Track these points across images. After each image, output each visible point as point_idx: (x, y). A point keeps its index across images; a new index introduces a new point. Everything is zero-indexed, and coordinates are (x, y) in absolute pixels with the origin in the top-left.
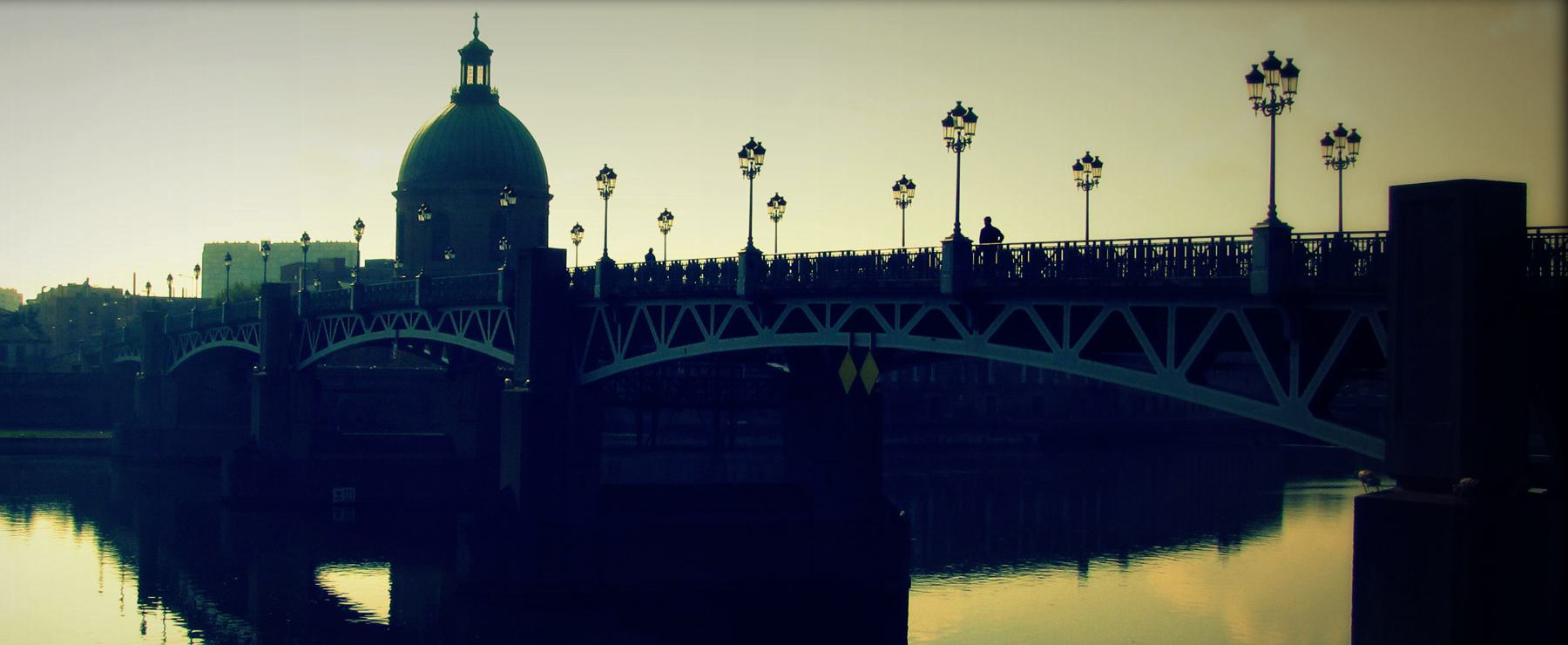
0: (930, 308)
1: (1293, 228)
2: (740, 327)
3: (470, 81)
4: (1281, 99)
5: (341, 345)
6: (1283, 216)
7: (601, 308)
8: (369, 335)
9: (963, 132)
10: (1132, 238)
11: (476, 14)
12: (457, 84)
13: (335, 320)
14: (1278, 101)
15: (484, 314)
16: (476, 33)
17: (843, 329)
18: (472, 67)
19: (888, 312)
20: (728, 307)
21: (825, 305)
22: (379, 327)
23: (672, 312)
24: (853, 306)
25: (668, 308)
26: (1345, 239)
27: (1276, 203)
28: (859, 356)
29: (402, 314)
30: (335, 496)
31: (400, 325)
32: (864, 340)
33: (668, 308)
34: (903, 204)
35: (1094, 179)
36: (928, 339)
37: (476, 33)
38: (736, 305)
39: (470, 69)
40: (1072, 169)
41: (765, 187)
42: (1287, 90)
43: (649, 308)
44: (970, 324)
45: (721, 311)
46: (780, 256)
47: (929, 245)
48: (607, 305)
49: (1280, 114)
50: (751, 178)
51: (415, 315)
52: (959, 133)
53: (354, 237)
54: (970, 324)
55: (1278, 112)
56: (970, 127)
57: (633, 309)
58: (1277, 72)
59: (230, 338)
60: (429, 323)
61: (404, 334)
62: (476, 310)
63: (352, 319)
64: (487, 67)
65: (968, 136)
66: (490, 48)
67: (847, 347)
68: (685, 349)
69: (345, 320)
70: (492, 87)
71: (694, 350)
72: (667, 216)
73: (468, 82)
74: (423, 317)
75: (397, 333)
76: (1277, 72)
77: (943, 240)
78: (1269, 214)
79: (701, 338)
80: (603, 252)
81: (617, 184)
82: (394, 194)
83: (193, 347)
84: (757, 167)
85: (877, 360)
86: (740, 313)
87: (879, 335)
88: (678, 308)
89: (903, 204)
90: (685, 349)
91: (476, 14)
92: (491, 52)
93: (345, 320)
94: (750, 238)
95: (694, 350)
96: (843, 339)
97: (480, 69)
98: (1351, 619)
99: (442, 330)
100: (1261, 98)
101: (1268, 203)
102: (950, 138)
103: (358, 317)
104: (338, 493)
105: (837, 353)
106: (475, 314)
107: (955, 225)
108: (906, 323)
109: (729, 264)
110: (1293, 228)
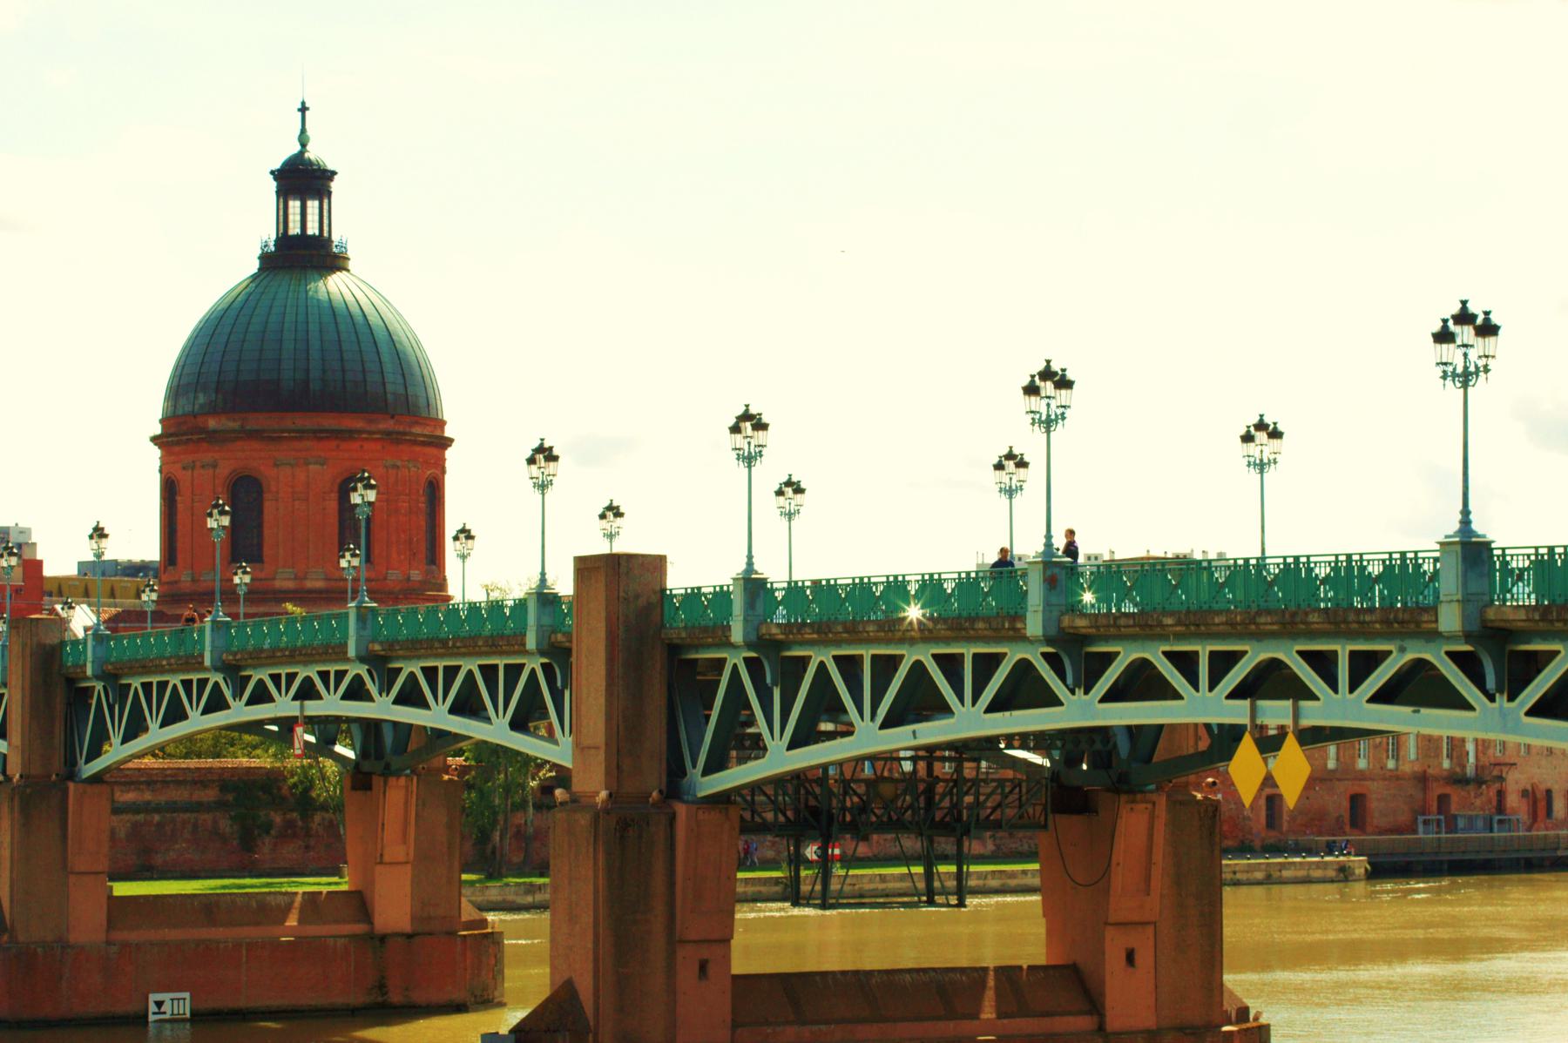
0: (1409, 656)
1: (1493, 542)
2: (216, 703)
3: (294, 229)
4: (1477, 367)
5: (178, 730)
6: (1482, 526)
7: (99, 686)
8: (239, 712)
9: (1053, 403)
10: (1235, 557)
11: (303, 103)
12: (270, 234)
13: (163, 685)
14: (1472, 369)
15: (489, 672)
16: (303, 140)
17: (294, 699)
18: (316, 203)
19: (1323, 663)
20: (458, 668)
21: (1335, 653)
22: (262, 696)
23: (886, 666)
24: (1255, 655)
25: (1213, 655)
26: (866, 584)
27: (753, 553)
28: (1269, 744)
29: (312, 672)
30: (152, 1008)
31: (307, 692)
32: (1275, 713)
33: (199, 680)
34: (790, 516)
35: (1018, 484)
36: (1407, 710)
37: (303, 140)
38: (911, 656)
39: (294, 205)
40: (774, 494)
41: (769, 474)
42: (1482, 354)
43: (424, 669)
44: (1070, 680)
45: (986, 665)
46: (796, 582)
47: (1409, 545)
48: (545, 660)
49: (1473, 386)
50: (1048, 432)
51: (340, 675)
52: (1048, 405)
53: (92, 553)
54: (1491, 683)
55: (1471, 383)
56: (1480, 345)
57: (804, 661)
58: (1471, 328)
59: (356, 692)
60: (228, 693)
61: (313, 708)
62: (470, 665)
63: (202, 683)
64: (326, 202)
65: (1062, 410)
66: (330, 167)
67: (1245, 726)
68: (914, 732)
69: (147, 687)
70: (335, 238)
71: (932, 732)
72: (544, 454)
73: (310, 232)
74: (358, 677)
75: (302, 707)
76: (1471, 328)
77: (1442, 539)
78: (1461, 522)
79: (944, 709)
80: (746, 560)
81: (561, 471)
82: (155, 439)
83: (153, 725)
84: (757, 450)
85: (1302, 742)
86: (1024, 667)
87: (1304, 704)
88: (521, 667)
89: (790, 516)
90: (914, 732)
91: (303, 103)
92: (331, 175)
93: (187, 684)
94: (1466, 512)
95: (932, 732)
96: (1238, 713)
97: (313, 206)
98: (139, 883)
99: (400, 700)
100: (1451, 364)
101: (746, 553)
102: (739, 449)
103: (217, 677)
104: (159, 1004)
105: (1226, 739)
106: (533, 671)
107: (1045, 537)
108: (291, 686)
109: (722, 596)
110: (1493, 542)
